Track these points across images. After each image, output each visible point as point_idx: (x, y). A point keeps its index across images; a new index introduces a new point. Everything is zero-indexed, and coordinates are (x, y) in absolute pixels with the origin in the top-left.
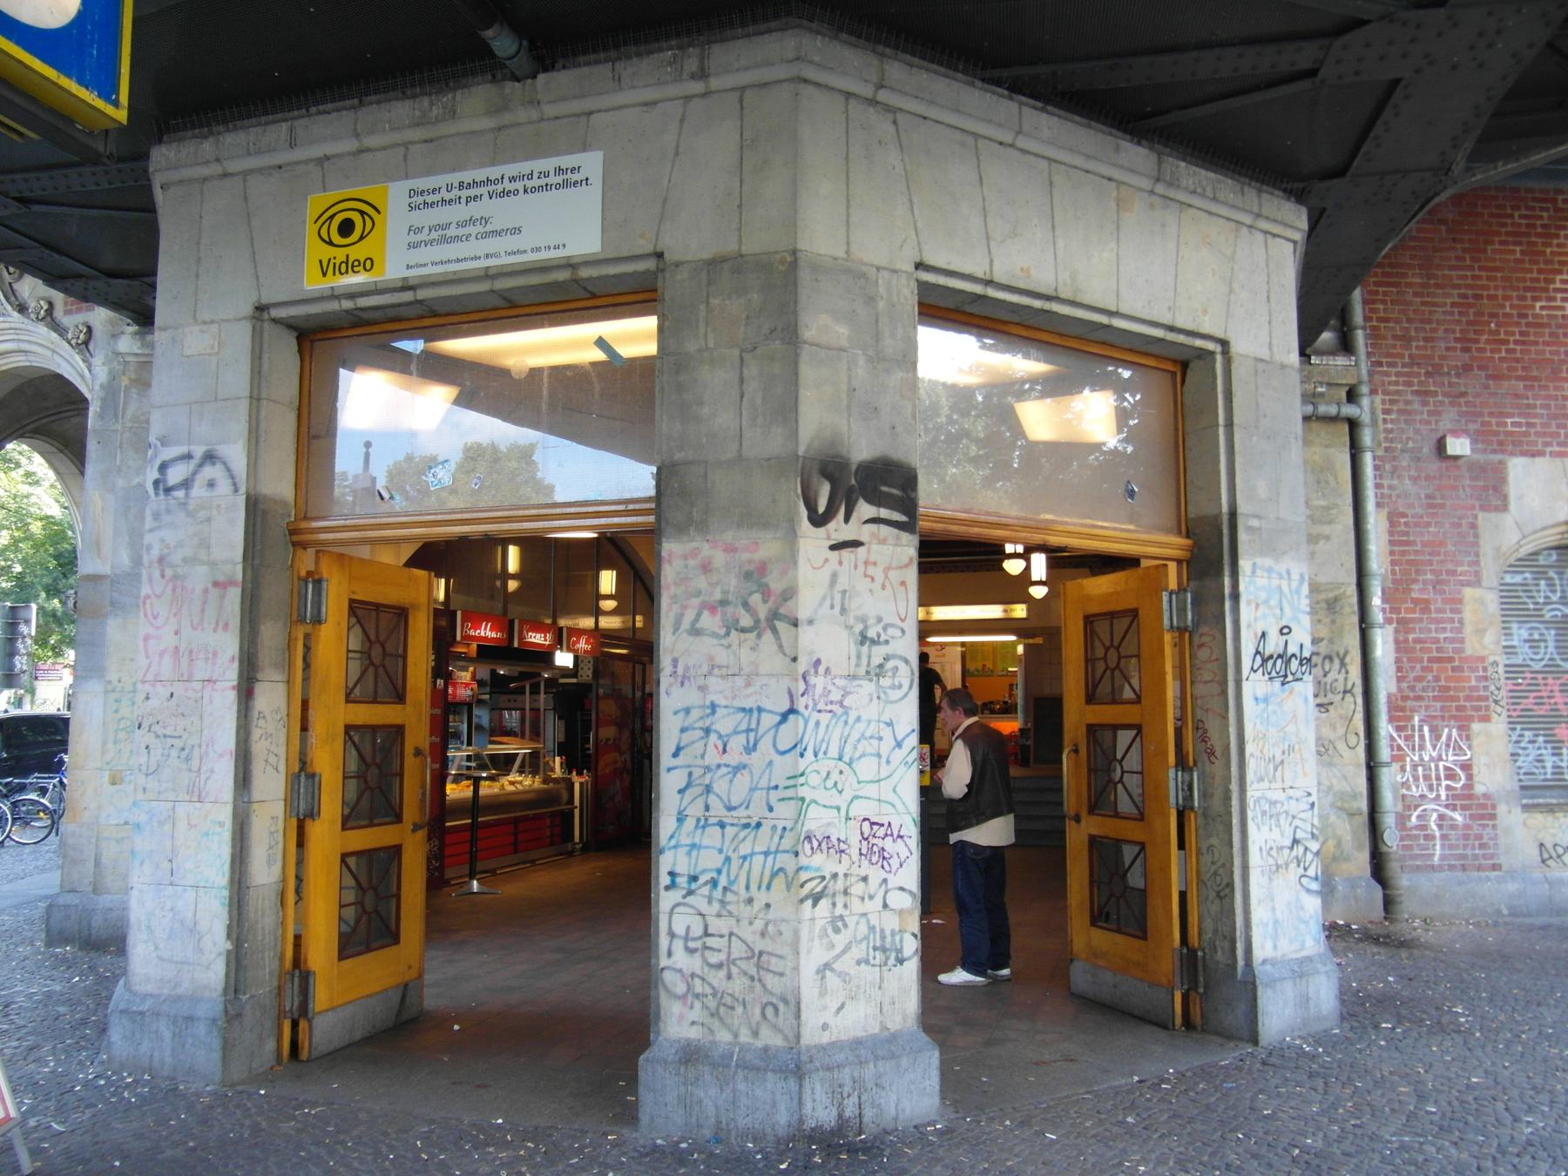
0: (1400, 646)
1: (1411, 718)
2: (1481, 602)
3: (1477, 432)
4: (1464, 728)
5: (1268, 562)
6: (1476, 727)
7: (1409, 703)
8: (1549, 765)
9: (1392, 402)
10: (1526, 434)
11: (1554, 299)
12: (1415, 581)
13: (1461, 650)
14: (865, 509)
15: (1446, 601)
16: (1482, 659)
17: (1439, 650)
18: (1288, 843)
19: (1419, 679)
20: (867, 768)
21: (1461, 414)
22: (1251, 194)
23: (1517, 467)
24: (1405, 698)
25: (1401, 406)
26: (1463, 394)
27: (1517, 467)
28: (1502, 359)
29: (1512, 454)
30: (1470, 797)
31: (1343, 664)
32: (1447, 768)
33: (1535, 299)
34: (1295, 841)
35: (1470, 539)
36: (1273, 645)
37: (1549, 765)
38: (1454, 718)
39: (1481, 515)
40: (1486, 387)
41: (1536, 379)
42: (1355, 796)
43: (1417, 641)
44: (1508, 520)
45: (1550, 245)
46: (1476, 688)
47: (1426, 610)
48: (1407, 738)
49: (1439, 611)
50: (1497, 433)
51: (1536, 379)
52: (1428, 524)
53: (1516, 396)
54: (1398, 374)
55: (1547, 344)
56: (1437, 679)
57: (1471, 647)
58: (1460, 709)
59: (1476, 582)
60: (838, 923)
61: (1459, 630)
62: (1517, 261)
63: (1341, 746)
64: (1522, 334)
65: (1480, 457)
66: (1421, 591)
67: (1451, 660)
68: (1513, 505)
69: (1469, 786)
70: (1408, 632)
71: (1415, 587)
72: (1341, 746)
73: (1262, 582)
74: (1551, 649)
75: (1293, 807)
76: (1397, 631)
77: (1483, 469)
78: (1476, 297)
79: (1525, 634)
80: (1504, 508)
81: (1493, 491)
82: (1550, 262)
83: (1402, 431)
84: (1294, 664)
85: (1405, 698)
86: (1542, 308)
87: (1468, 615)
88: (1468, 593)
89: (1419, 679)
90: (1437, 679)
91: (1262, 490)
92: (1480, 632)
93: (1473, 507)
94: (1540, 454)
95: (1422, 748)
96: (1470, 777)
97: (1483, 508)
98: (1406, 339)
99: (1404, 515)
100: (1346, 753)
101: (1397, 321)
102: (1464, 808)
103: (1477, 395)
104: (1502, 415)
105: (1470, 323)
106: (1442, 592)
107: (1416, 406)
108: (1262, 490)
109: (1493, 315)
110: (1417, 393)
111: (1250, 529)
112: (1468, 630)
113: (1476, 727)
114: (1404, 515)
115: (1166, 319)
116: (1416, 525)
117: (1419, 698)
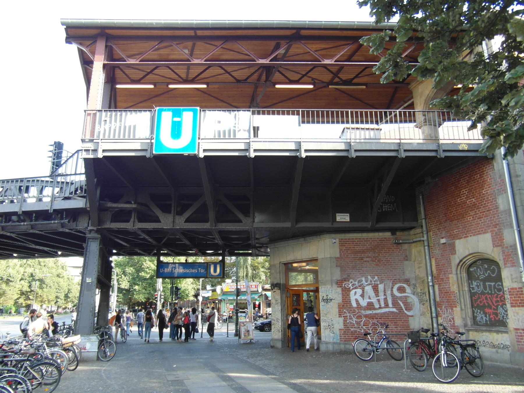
0: (440, 290)
1: (442, 307)
2: (453, 277)
3: (449, 236)
4: (452, 309)
5: (324, 286)
6: (454, 309)
7: (442, 303)
8: (484, 319)
9: (434, 232)
10: (458, 234)
11: (461, 197)
12: (440, 274)
13: (450, 290)
14: (276, 288)
15: (447, 278)
16: (454, 292)
17: (446, 290)
18: (328, 325)
19: (443, 297)
20: (277, 313)
21: (446, 232)
22: (318, 236)
23: (457, 242)
24: (441, 302)
25: (435, 233)
26: (446, 227)
27: (457, 242)
28: (452, 216)
29: (456, 239)
30: (454, 326)
31: (426, 295)
32: (450, 319)
33: (458, 198)
34: (329, 325)
35: (449, 262)
36: (325, 298)
37: (484, 319)
38: (450, 306)
39: (451, 256)
40: (450, 224)
41: (459, 219)
42: (429, 324)
43: (442, 288)
44: (456, 256)
45: (459, 184)
46: (453, 299)
47: (443, 281)
48: (442, 311)
49: (446, 281)
50: (453, 235)
51: (459, 219)
52: (442, 260)
53: (456, 225)
54: (434, 226)
55: (461, 209)
56: (446, 297)
57: (452, 289)
58: (451, 304)
59: (451, 273)
60: (275, 327)
61: (449, 285)
62: (453, 190)
63: (426, 313)
64: (456, 208)
65: (450, 242)
66: (442, 276)
67: (448, 292)
68: (457, 253)
69: (454, 324)
70: (440, 286)
71: (441, 275)
72: (426, 313)
73: (323, 289)
74: (482, 287)
75: (329, 320)
76: (438, 286)
77: (451, 245)
78: (446, 202)
79: (476, 284)
80: (455, 254)
81: (452, 249)
82: (460, 188)
83: (436, 239)
84: (329, 300)
85: (441, 302)
86: (459, 200)
87: (450, 281)
88: (450, 276)
89: (443, 297)
90: (446, 297)
91: (323, 276)
92: (453, 285)
93: (449, 255)
94: (461, 238)
95: (445, 314)
96: (454, 321)
97: (452, 254)
98: (435, 217)
99: (437, 259)
100: (427, 314)
101: (433, 213)
102: (454, 329)
103: (448, 227)
104: (453, 230)
105: (446, 209)
106: (446, 276)
107: (438, 233)
108: (323, 276)
109: (450, 206)
110: (438, 229)
111: (321, 282)
112: (451, 285)
113: (454, 309)
114: (437, 259)
115: (308, 257)
116: (440, 261)
117: (443, 302)
